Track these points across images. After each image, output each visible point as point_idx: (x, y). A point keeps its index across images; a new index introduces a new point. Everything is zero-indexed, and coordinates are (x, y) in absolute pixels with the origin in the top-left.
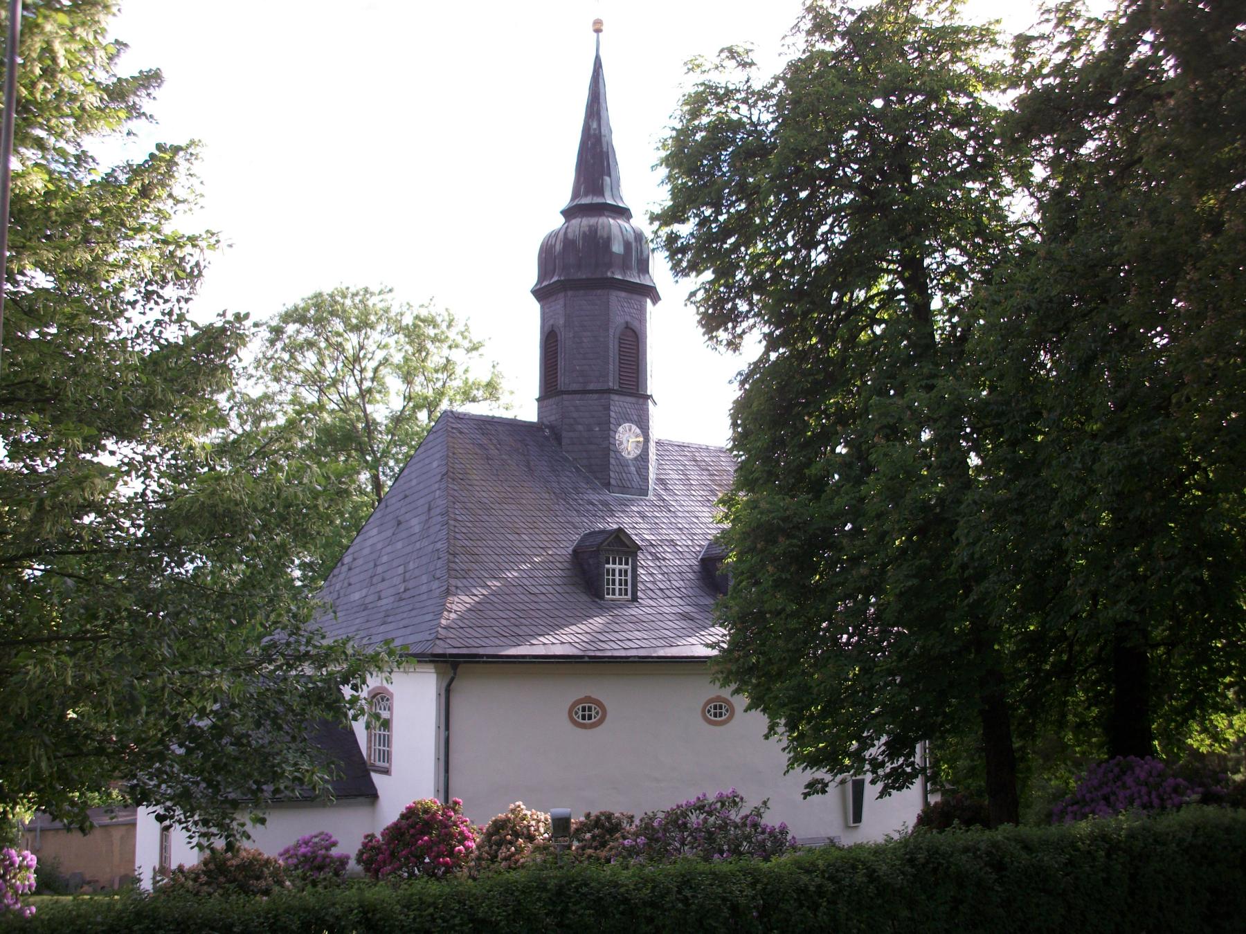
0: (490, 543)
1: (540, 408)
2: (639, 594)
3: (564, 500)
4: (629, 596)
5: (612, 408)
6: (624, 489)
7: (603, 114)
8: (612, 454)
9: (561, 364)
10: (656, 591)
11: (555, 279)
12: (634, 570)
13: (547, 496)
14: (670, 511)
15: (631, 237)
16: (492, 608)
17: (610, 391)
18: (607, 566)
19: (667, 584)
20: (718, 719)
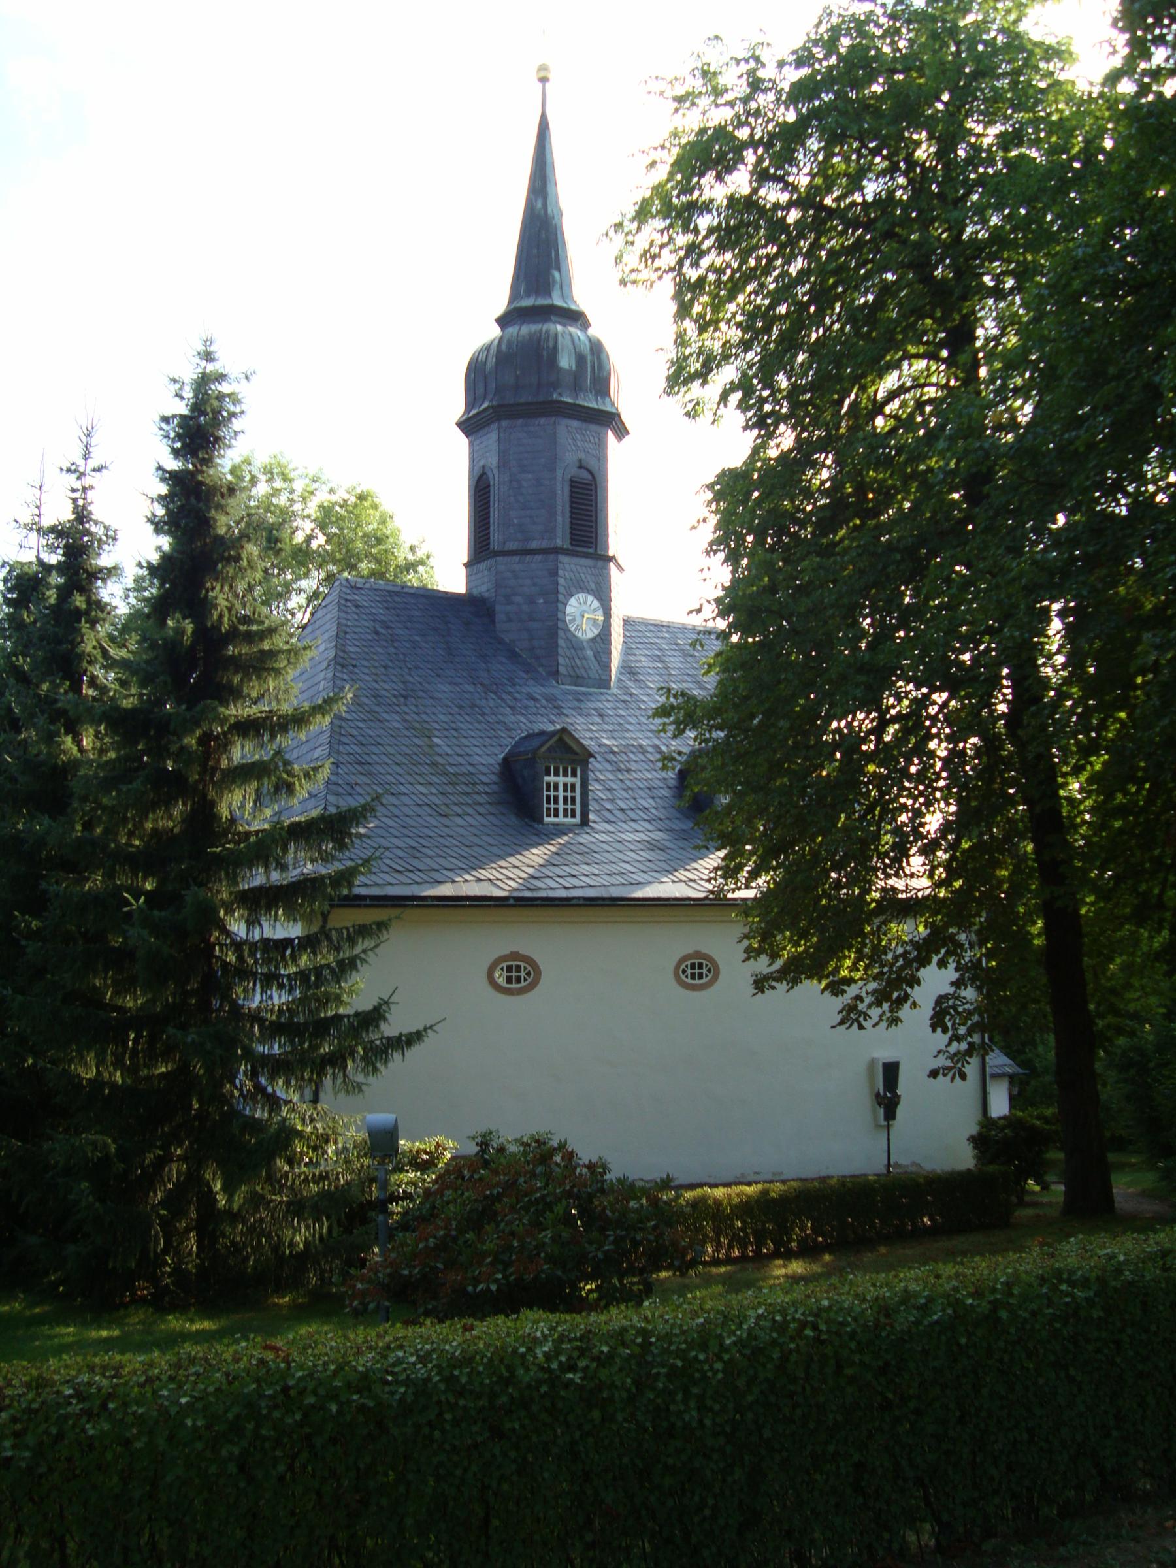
0: (389, 748)
1: (468, 576)
2: (592, 817)
3: (495, 693)
4: (577, 820)
5: (560, 572)
6: (577, 680)
7: (550, 189)
8: (561, 633)
9: (494, 515)
10: (615, 812)
11: (485, 405)
12: (584, 784)
13: (471, 688)
14: (640, 708)
15: (586, 348)
16: (385, 834)
17: (557, 551)
18: (547, 779)
19: (632, 803)
20: (697, 982)
